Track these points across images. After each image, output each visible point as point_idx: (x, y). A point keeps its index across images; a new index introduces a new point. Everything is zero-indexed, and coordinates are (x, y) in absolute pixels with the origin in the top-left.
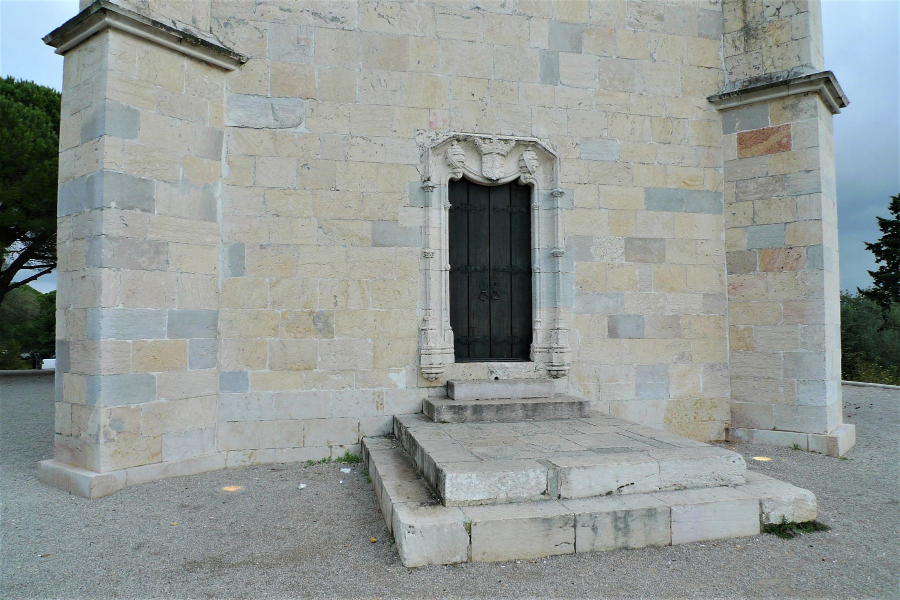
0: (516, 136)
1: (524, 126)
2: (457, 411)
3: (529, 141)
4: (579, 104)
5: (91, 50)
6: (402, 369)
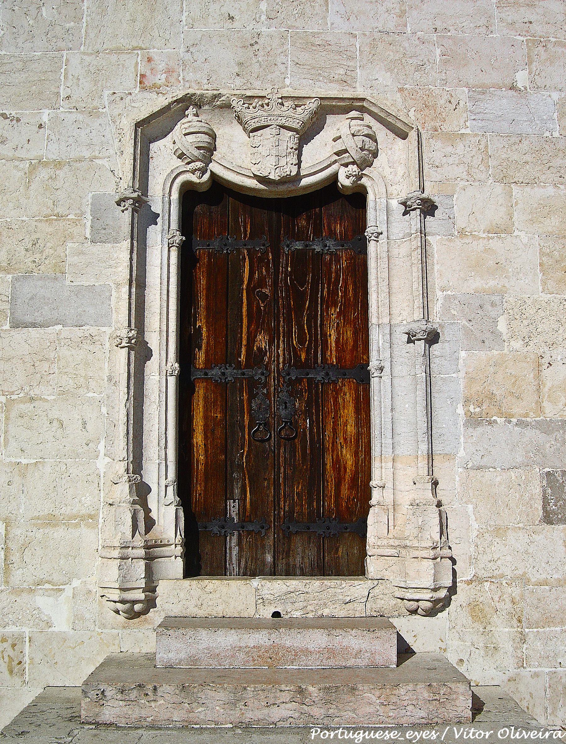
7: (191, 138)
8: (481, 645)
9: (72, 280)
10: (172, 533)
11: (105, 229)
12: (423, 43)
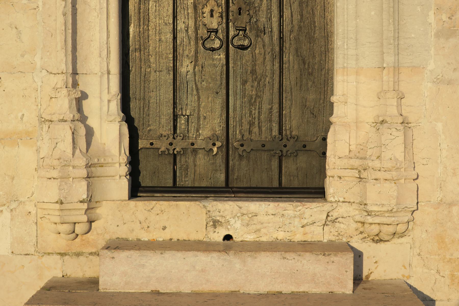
5: (261, 204)
8: (447, 273)
10: (115, 151)
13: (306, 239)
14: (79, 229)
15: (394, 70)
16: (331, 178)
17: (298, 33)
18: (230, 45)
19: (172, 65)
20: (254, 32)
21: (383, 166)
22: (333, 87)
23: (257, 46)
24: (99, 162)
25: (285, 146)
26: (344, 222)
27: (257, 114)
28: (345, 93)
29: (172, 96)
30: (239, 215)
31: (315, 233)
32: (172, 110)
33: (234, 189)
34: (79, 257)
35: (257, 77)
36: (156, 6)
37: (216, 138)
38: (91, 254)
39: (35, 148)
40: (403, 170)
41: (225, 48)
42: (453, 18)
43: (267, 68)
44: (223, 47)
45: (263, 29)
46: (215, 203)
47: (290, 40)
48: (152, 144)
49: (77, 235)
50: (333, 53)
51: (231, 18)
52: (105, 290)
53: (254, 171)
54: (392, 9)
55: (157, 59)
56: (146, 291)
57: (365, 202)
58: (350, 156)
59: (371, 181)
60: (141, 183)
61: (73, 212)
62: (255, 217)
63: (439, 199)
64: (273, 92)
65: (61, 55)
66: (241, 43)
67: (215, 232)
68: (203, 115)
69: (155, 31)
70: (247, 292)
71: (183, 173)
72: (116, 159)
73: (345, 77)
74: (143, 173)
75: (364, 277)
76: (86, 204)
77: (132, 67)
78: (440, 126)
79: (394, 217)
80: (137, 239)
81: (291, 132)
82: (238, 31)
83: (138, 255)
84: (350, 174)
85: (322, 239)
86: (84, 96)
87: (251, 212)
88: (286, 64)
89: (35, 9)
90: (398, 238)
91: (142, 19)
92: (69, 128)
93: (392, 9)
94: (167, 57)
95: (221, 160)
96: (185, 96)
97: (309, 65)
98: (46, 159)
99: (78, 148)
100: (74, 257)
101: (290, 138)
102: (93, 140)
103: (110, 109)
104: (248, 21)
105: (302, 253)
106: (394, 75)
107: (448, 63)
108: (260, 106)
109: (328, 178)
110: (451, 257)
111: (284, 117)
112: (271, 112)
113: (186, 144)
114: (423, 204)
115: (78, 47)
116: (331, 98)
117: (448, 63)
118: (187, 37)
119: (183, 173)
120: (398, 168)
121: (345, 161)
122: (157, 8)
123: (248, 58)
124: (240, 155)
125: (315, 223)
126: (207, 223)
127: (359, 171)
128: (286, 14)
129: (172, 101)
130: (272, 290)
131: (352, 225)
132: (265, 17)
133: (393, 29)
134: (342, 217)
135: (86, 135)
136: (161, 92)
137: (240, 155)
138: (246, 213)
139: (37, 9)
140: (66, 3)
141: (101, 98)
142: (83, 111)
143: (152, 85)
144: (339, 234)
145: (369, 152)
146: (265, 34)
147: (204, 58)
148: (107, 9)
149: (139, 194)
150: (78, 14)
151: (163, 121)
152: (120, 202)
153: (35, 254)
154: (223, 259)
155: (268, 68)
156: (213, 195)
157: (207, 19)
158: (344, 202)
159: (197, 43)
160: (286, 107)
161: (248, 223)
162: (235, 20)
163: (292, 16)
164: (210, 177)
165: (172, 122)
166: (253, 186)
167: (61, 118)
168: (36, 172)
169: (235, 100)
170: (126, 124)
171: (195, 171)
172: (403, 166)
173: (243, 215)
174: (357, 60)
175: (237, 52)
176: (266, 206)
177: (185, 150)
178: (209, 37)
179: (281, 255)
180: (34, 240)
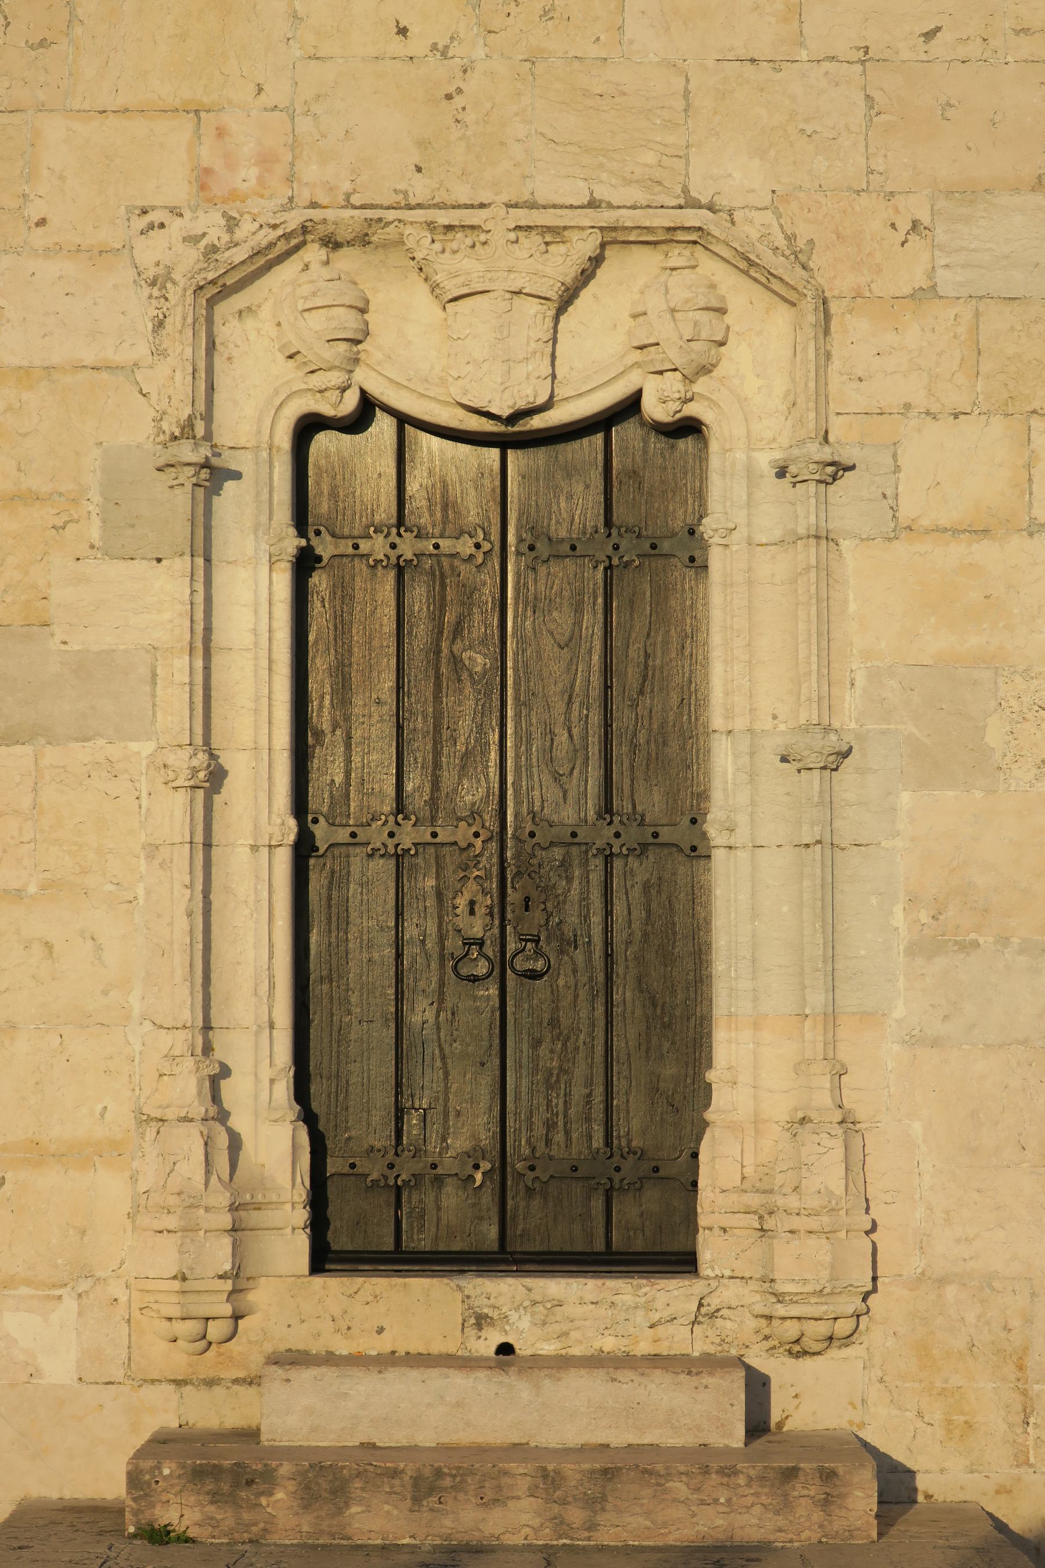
0: (610, 206)
1: (650, 158)
2: (226, 1487)
3: (669, 229)
4: (929, 35)
6: (60, 1297)
7: (316, 322)
8: (938, 1416)
9: (65, 638)
10: (283, 1178)
11: (133, 526)
12: (837, 85)
13: (658, 1352)
14: (215, 1331)
15: (825, 1021)
16: (706, 1231)
17: (642, 946)
18: (509, 971)
19: (393, 1010)
20: (555, 944)
21: (805, 1206)
22: (710, 1052)
23: (562, 972)
24: (253, 1201)
25: (618, 1169)
26: (732, 1317)
27: (561, 1106)
28: (733, 1064)
29: (394, 1070)
30: (526, 1303)
31: (676, 1339)
32: (393, 1099)
33: (517, 1256)
34: (213, 1388)
35: (560, 1034)
36: (362, 893)
37: (480, 1153)
38: (236, 1381)
39: (127, 1174)
40: (842, 1213)
41: (498, 976)
42: (941, 917)
43: (581, 1014)
44: (494, 973)
45: (572, 939)
46: (479, 1280)
47: (626, 960)
48: (353, 1166)
49: (210, 1343)
50: (710, 986)
51: (509, 916)
52: (272, 1443)
53: (555, 1220)
54: (819, 904)
55: (365, 997)
56: (351, 1444)
57: (771, 1277)
58: (744, 1187)
59: (783, 1234)
60: (332, 1245)
61: (206, 1298)
62: (559, 1308)
63: (919, 1270)
64: (593, 1063)
65: (183, 993)
66: (530, 965)
67: (480, 1337)
68: (455, 1108)
69: (361, 943)
70: (544, 1446)
71: (415, 1225)
72: (287, 1196)
73: (733, 1034)
74: (335, 1224)
75: (773, 1425)
76: (230, 1282)
77: (315, 1013)
78: (917, 1127)
79: (826, 1304)
80: (327, 1352)
81: (629, 1141)
82: (523, 943)
83: (335, 1374)
84: (742, 1224)
85: (689, 1351)
86: (225, 1071)
87: (551, 1298)
88: (618, 1007)
89: (131, 902)
90: (840, 1347)
91: (334, 919)
92: (199, 1133)
93: (820, 903)
94: (384, 995)
95: (490, 1198)
96: (419, 1071)
97: (663, 1009)
98: (152, 1194)
99: (214, 1172)
100: (202, 1387)
101: (628, 1153)
102: (241, 1158)
103: (274, 1097)
104: (542, 922)
105: (647, 1371)
106: (825, 1029)
107: (932, 1005)
108: (568, 1090)
109: (701, 1230)
110: (944, 1386)
111: (614, 1112)
112: (589, 1102)
113: (421, 1165)
114: (887, 1280)
115: (214, 976)
116: (707, 1074)
117: (932, 1005)
118: (423, 954)
119: (415, 1225)
120: (833, 1210)
121: (734, 1197)
122: (365, 897)
123: (543, 996)
124: (528, 1188)
125: (675, 1318)
126: (464, 1320)
127: (761, 1217)
128: (618, 908)
129: (394, 1081)
130: (591, 1442)
131: (748, 1322)
132: (576, 914)
133: (822, 941)
134: (729, 1308)
135: (229, 1147)
136: (371, 1061)
137: (528, 1188)
138: (539, 1301)
139: (135, 903)
140: (192, 892)
141: (256, 1075)
142: (221, 1100)
143: (353, 1049)
144: (723, 1340)
145: (779, 1179)
146: (576, 948)
147: (457, 996)
148: (269, 902)
149: (327, 1267)
150: (212, 913)
151: (376, 1120)
152: (293, 1279)
153: (127, 1382)
154: (496, 1382)
155: (584, 1014)
156: (474, 1268)
157: (462, 920)
158: (732, 1278)
159: (442, 966)
160: (618, 1091)
161: (544, 1320)
162: (519, 920)
163: (630, 914)
164: (468, 1231)
165: (393, 1123)
166: (555, 1249)
167: (183, 1115)
168: (129, 1221)
169: (519, 1079)
170: (306, 1127)
171: (439, 1220)
172: (844, 1205)
173: (535, 1303)
174: (755, 999)
175: (522, 984)
176: (580, 1287)
177: (418, 1177)
178: (467, 954)
179: (608, 1373)
180: (124, 1355)
